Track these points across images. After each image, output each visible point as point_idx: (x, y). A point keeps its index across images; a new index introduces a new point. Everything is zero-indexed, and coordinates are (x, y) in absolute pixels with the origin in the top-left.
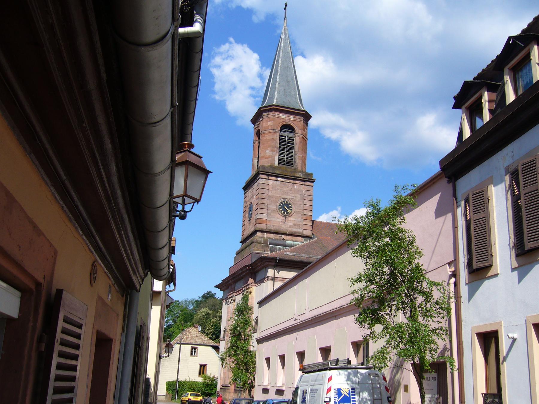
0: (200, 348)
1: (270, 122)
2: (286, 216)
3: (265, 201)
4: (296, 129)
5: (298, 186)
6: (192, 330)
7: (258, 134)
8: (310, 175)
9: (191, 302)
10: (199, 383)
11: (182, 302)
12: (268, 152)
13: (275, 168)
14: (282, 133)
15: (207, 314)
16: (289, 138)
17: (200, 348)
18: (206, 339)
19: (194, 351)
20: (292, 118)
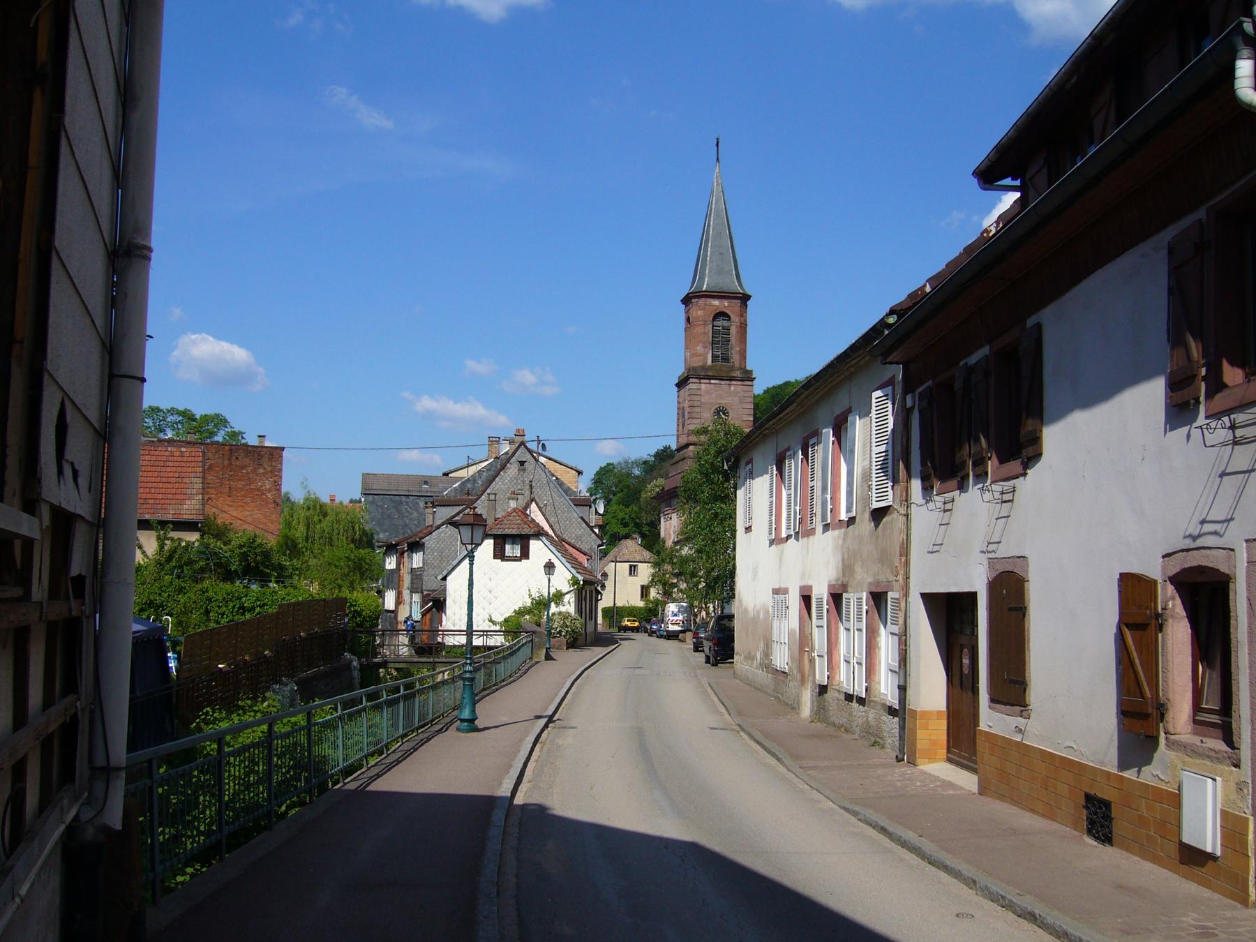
1: (702, 310)
3: (697, 410)
5: (736, 387)
6: (629, 542)
7: (688, 319)
8: (750, 372)
9: (636, 463)
11: (619, 463)
12: (699, 349)
13: (710, 368)
18: (647, 555)
19: (633, 571)
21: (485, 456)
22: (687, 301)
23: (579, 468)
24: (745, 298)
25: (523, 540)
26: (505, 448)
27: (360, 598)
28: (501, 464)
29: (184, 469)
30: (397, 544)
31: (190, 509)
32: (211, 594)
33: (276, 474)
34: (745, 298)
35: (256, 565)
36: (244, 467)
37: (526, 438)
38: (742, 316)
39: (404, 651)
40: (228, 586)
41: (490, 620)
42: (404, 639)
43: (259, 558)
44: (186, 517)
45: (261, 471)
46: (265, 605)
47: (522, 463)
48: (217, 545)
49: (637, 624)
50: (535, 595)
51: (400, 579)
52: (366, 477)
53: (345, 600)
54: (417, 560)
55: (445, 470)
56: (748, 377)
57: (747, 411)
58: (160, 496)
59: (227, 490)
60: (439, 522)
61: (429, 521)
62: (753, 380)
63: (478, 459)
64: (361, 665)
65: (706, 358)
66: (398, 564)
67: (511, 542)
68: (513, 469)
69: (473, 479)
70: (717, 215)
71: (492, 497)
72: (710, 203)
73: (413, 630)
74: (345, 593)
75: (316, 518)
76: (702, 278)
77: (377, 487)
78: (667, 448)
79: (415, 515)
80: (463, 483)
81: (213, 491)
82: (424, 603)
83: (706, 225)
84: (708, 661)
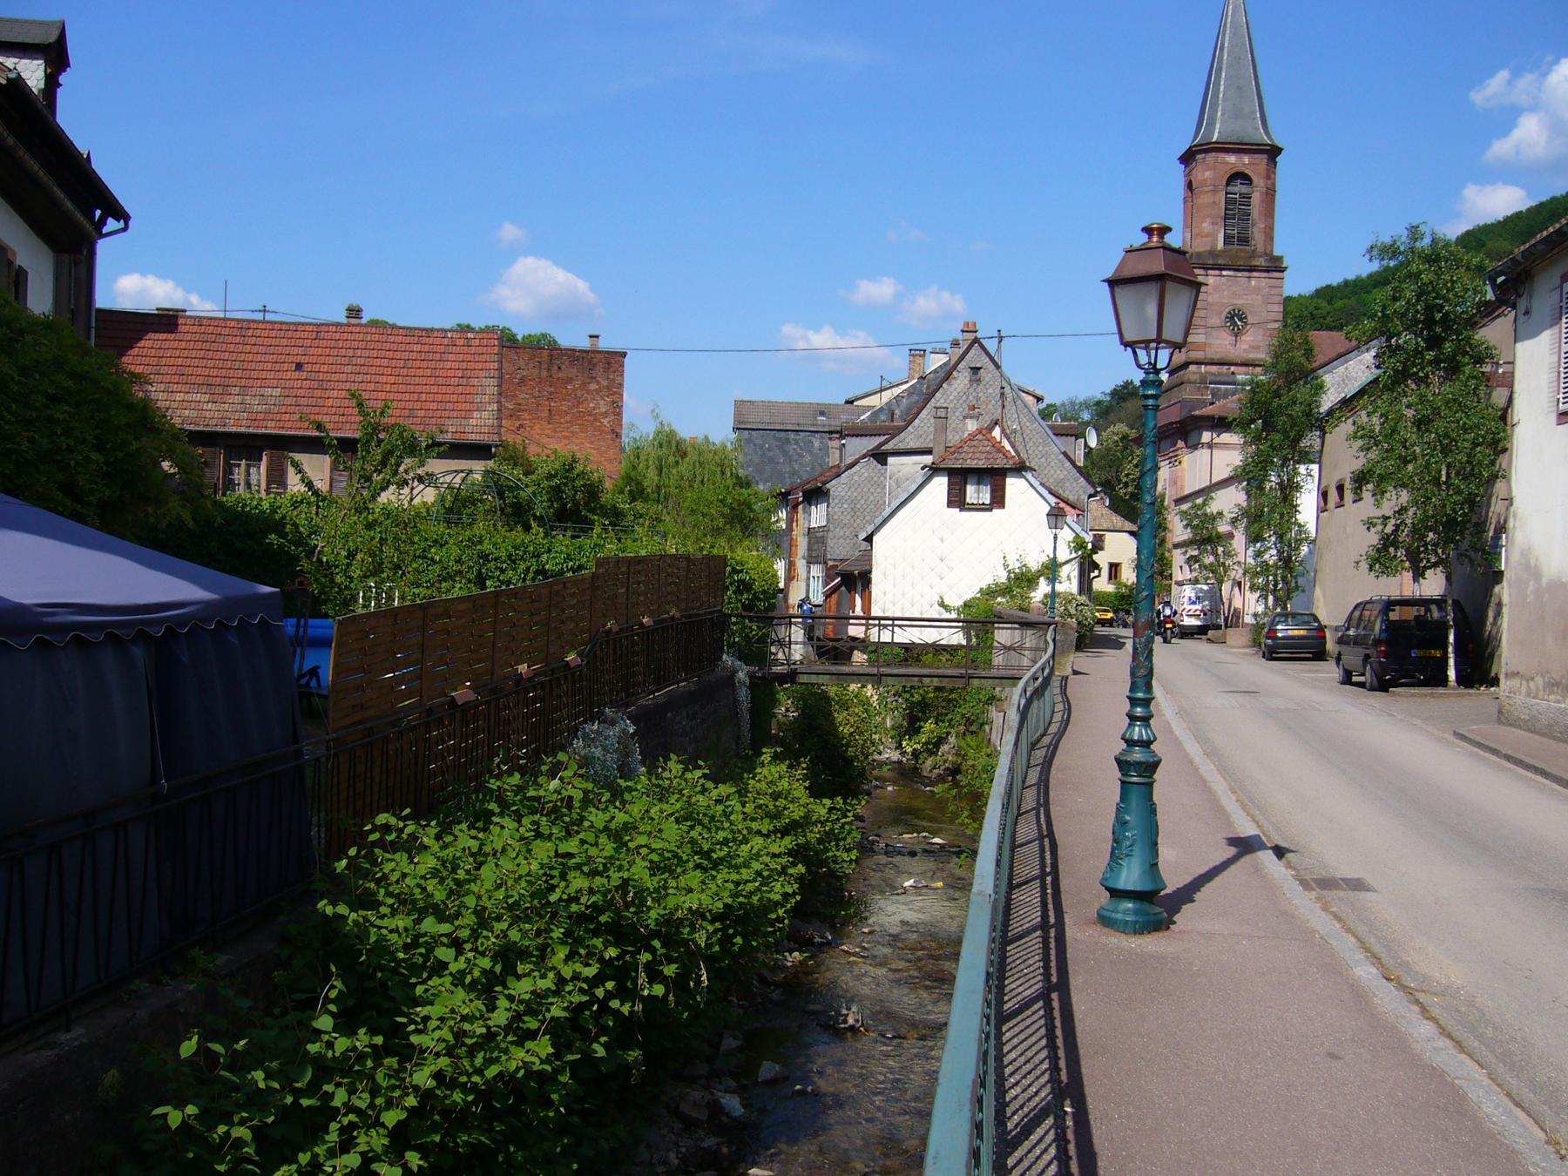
0: (1109, 536)
1: (1210, 171)
2: (1237, 334)
4: (1255, 179)
5: (1258, 281)
7: (1190, 185)
8: (1280, 259)
9: (1085, 405)
10: (1109, 594)
11: (1063, 405)
12: (1206, 226)
14: (1230, 189)
15: (1124, 438)
16: (1243, 196)
17: (1109, 536)
18: (1118, 521)
20: (1246, 159)
21: (904, 376)
22: (1187, 158)
23: (1039, 393)
24: (1273, 152)
25: (995, 477)
26: (935, 362)
27: (746, 555)
28: (927, 389)
29: (472, 365)
30: (788, 493)
31: (479, 425)
32: (486, 547)
33: (614, 390)
34: (1273, 152)
35: (575, 503)
36: (570, 380)
37: (979, 335)
38: (1268, 177)
39: (797, 652)
40: (518, 535)
41: (942, 604)
42: (798, 634)
43: (579, 496)
44: (473, 438)
45: (593, 386)
46: (581, 567)
47: (976, 370)
48: (513, 474)
49: (1110, 615)
50: (1014, 565)
51: (792, 544)
52: (740, 405)
53: (723, 560)
54: (818, 516)
55: (850, 396)
56: (1275, 266)
57: (1273, 316)
58: (434, 406)
59: (545, 414)
60: (849, 460)
61: (833, 459)
62: (1283, 270)
63: (895, 381)
64: (751, 676)
65: (1216, 239)
66: (790, 521)
67: (976, 479)
68: (961, 379)
69: (889, 409)
70: (1234, 34)
71: (942, 413)
72: (1223, 15)
73: (811, 619)
74: (721, 548)
75: (671, 459)
76: (1211, 124)
77: (754, 419)
78: (1127, 384)
79: (808, 458)
80: (875, 414)
81: (526, 415)
82: (828, 579)
83: (1218, 47)
84: (1347, 679)
